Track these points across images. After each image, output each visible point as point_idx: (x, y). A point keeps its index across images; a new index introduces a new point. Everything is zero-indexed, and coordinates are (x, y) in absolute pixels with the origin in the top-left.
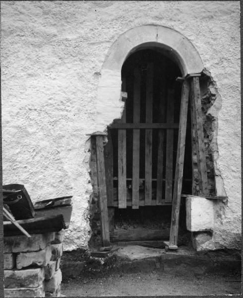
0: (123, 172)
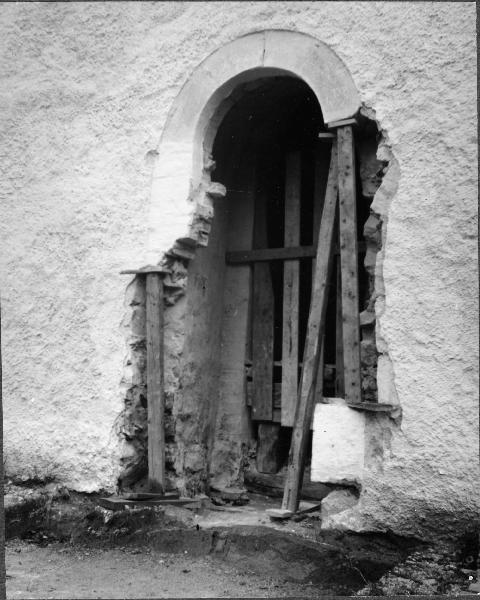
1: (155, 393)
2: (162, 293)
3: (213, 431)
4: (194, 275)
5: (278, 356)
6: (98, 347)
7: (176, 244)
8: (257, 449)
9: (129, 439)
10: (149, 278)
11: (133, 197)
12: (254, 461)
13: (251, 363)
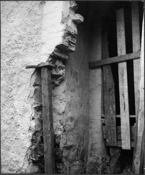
0: (125, 109)
1: (47, 135)
2: (50, 78)
3: (87, 152)
4: (70, 70)
5: (118, 112)
6: (18, 110)
7: (56, 49)
8: (110, 160)
9: (34, 162)
10: (42, 70)
11: (33, 28)
12: (109, 167)
13: (104, 116)
